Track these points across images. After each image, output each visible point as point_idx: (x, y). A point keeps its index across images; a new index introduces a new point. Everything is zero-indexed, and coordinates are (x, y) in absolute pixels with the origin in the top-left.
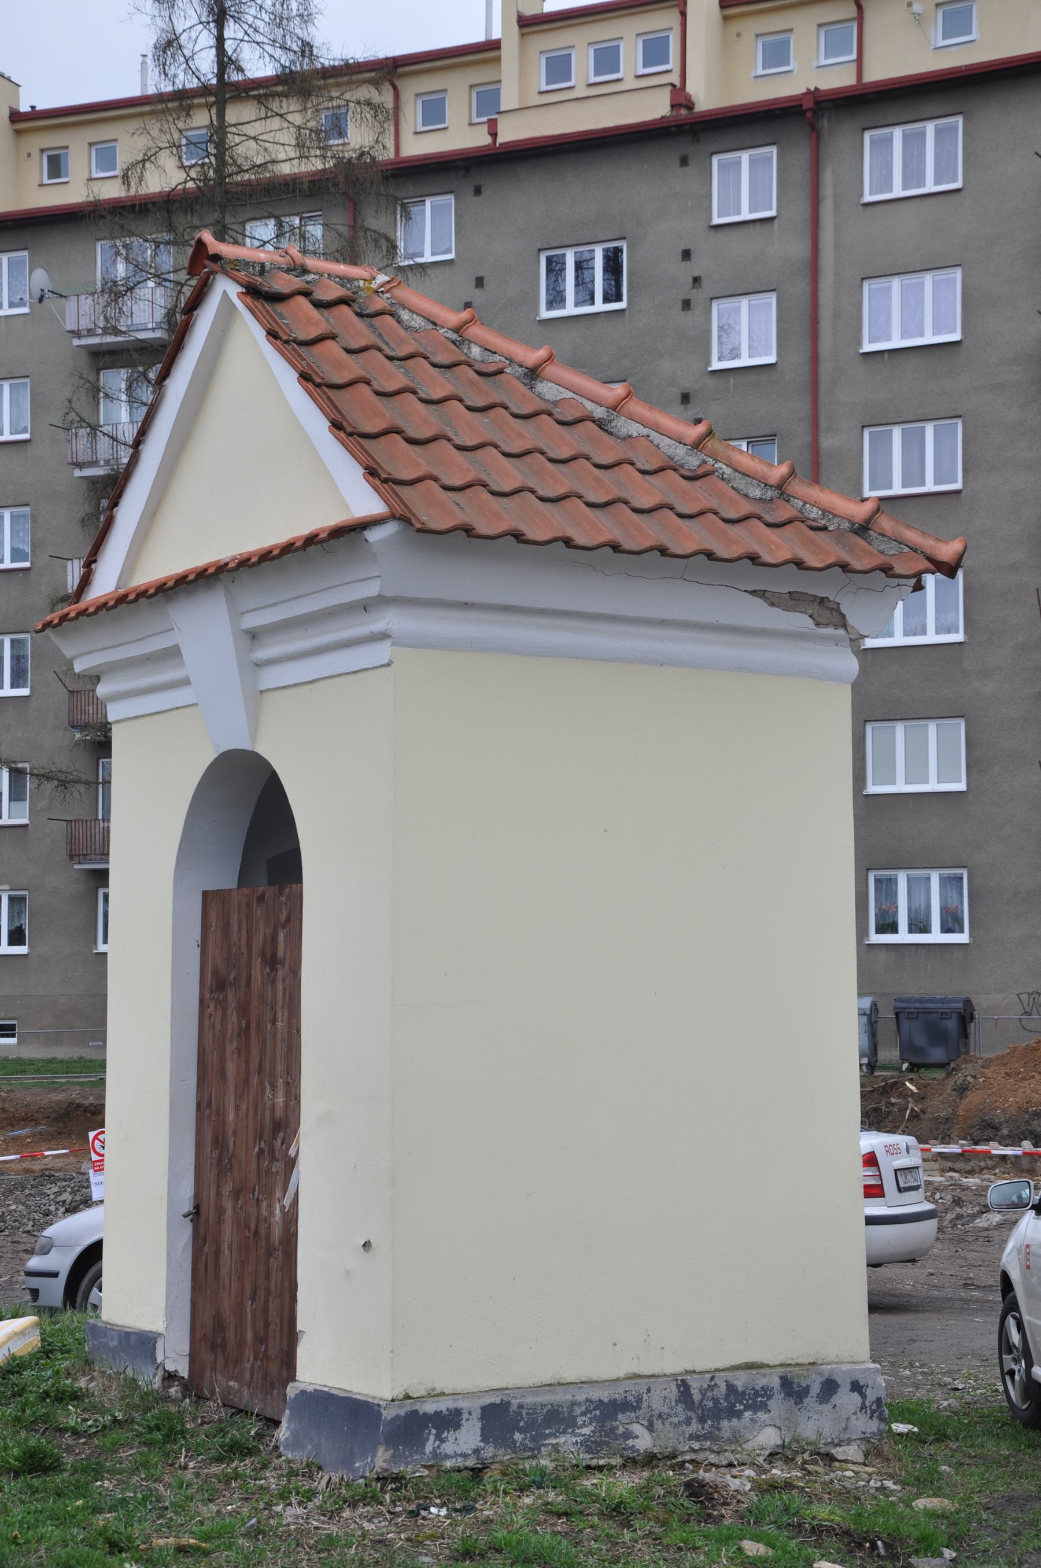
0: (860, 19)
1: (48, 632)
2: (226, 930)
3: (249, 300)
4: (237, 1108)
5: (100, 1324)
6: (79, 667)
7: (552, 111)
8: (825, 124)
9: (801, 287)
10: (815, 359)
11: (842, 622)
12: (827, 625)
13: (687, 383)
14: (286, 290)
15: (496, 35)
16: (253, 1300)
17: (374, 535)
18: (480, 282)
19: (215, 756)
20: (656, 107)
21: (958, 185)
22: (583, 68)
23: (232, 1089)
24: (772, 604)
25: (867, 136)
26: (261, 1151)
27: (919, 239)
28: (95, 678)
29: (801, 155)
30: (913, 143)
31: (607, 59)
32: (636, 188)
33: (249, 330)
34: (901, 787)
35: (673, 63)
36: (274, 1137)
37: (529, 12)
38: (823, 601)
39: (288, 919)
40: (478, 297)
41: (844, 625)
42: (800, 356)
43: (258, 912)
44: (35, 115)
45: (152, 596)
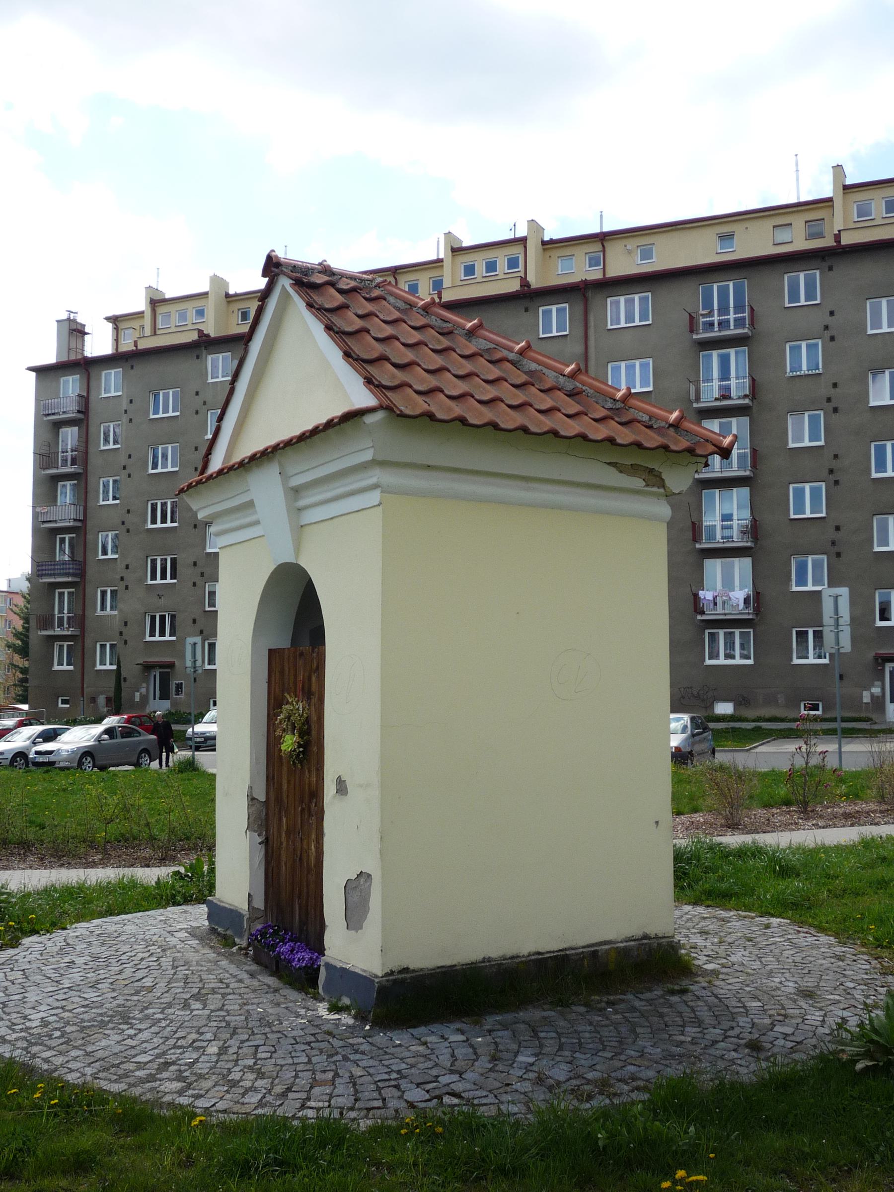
0: (604, 251)
1: (183, 495)
2: (282, 672)
3: (296, 288)
4: (289, 782)
5: (215, 901)
6: (200, 516)
7: (466, 288)
8: (589, 294)
11: (662, 484)
12: (653, 486)
14: (319, 281)
15: (442, 256)
16: (299, 898)
17: (369, 419)
19: (273, 567)
20: (514, 286)
21: (650, 322)
22: (480, 269)
23: (285, 769)
24: (621, 472)
25: (609, 300)
26: (303, 810)
27: (634, 345)
28: (208, 524)
29: (580, 308)
30: (630, 303)
31: (491, 266)
33: (298, 303)
36: (311, 802)
37: (455, 246)
38: (651, 471)
39: (318, 667)
41: (664, 486)
43: (300, 663)
44: (552, 242)
45: (237, 469)
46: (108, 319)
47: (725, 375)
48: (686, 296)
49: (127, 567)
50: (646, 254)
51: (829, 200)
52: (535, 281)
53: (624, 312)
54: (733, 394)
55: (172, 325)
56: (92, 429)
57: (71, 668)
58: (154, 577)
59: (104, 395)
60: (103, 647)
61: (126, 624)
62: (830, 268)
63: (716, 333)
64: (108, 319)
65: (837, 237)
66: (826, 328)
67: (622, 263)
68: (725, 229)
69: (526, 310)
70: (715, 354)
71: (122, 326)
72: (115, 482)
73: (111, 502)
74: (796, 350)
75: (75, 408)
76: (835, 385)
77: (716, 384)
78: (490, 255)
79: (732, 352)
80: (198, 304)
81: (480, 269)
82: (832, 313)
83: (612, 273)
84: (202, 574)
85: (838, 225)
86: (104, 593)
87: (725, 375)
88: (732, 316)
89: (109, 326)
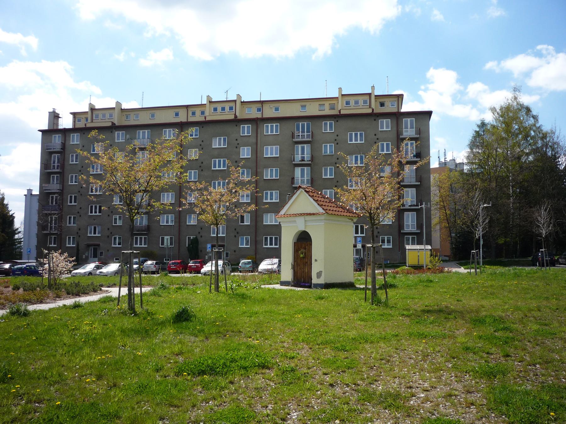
9: (255, 146)
10: (257, 157)
13: (237, 160)
18: (203, 141)
20: (232, 117)
22: (219, 109)
27: (273, 141)
29: (255, 127)
31: (223, 109)
32: (229, 128)
34: (269, 156)
35: (234, 110)
40: (202, 143)
42: (254, 156)
44: (244, 102)
46: (71, 113)
47: (303, 153)
48: (290, 126)
49: (81, 208)
50: (277, 109)
51: (337, 98)
52: (239, 117)
53: (270, 130)
54: (305, 160)
55: (99, 118)
56: (66, 156)
57: (55, 246)
58: (91, 212)
59: (71, 143)
60: (69, 238)
61: (80, 229)
62: (337, 121)
63: (300, 140)
64: (71, 113)
65: (340, 111)
66: (336, 140)
67: (269, 113)
68: (303, 104)
69: (375, 120)
70: (300, 146)
71: (77, 116)
72: (76, 176)
73: (74, 183)
74: (326, 146)
75: (60, 147)
76: (338, 159)
77: (300, 156)
78: (223, 105)
79: (305, 145)
80: (111, 111)
81: (219, 109)
82: (337, 136)
83: (265, 116)
84: (112, 212)
85: (340, 108)
86: (70, 218)
87: (303, 153)
88: (306, 134)
89: (72, 116)
